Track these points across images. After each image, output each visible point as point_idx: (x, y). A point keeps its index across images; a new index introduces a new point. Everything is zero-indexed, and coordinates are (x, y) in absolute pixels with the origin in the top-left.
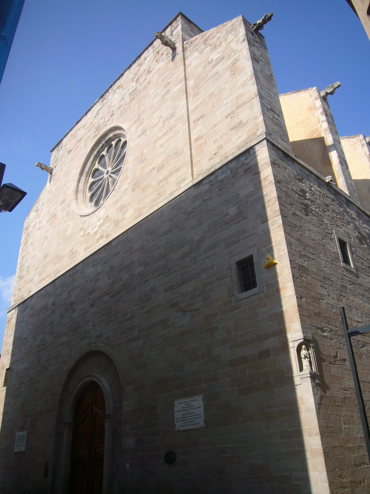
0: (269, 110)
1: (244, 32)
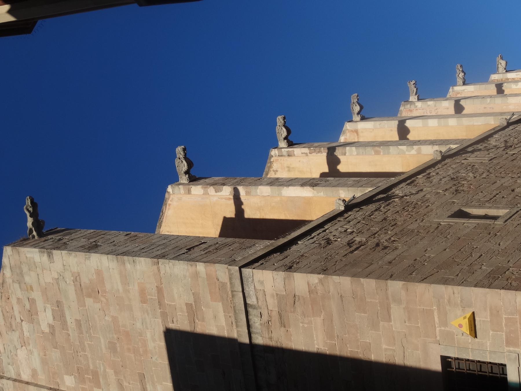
0: (190, 253)
1: (37, 250)
